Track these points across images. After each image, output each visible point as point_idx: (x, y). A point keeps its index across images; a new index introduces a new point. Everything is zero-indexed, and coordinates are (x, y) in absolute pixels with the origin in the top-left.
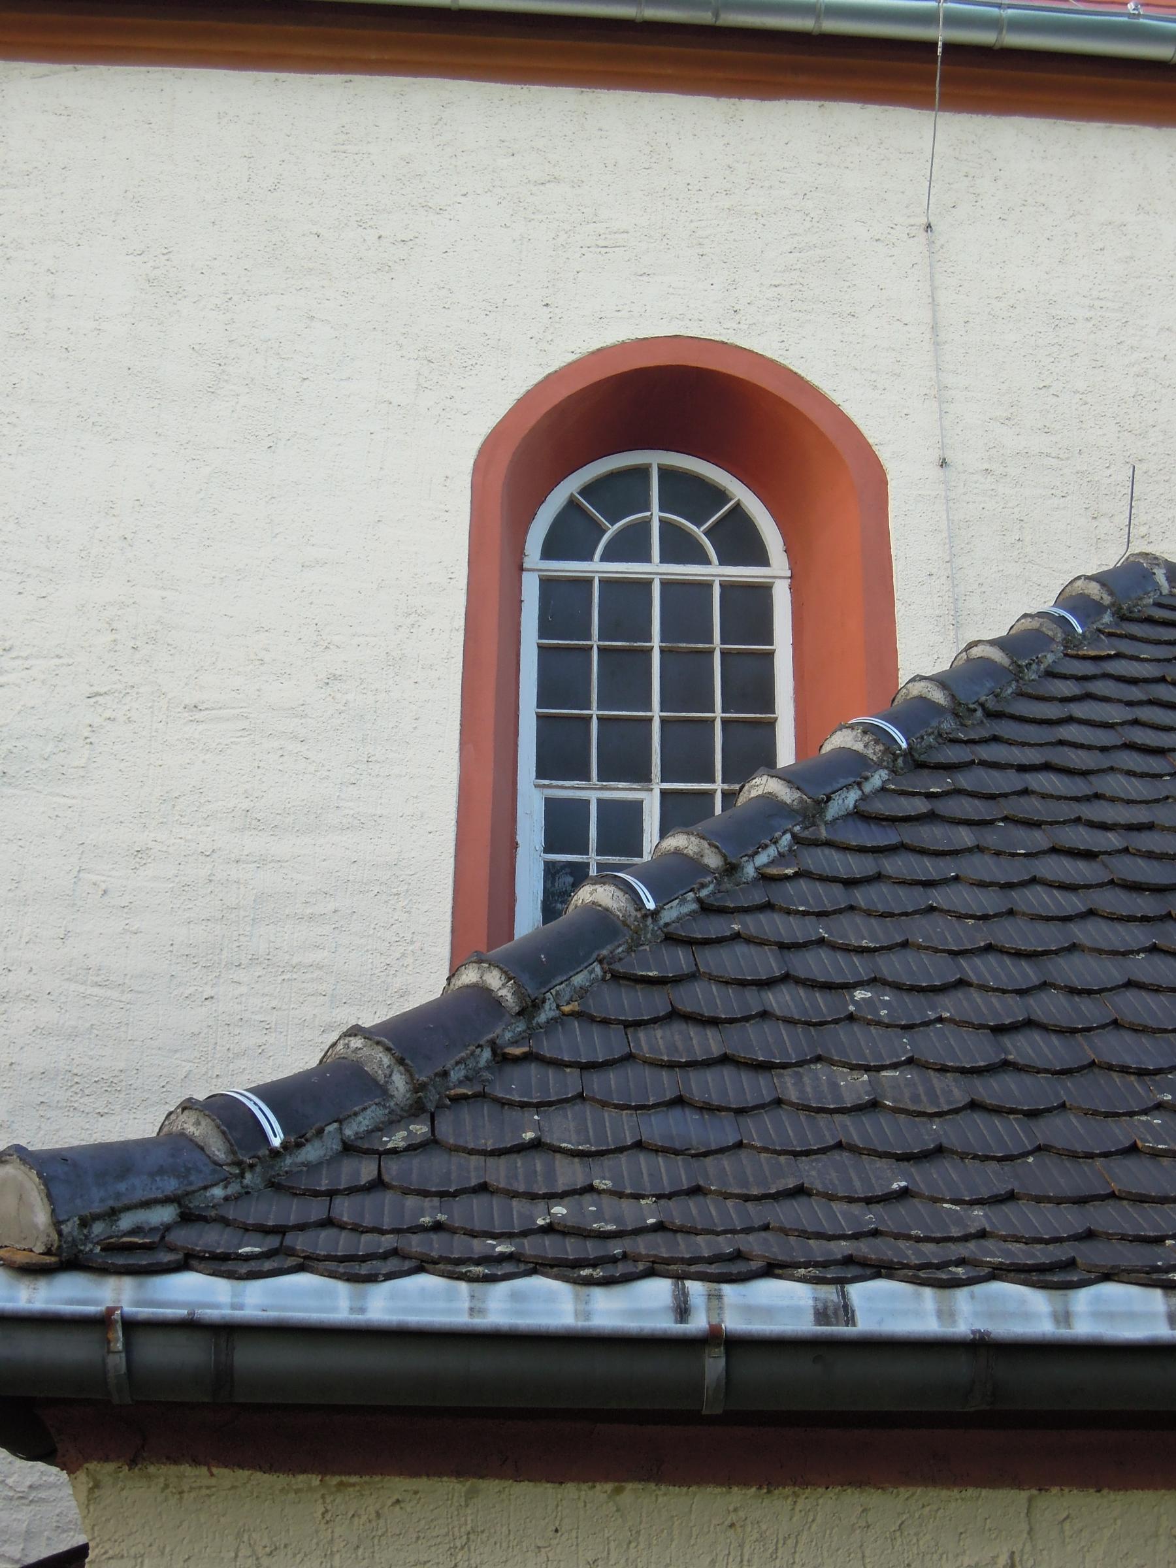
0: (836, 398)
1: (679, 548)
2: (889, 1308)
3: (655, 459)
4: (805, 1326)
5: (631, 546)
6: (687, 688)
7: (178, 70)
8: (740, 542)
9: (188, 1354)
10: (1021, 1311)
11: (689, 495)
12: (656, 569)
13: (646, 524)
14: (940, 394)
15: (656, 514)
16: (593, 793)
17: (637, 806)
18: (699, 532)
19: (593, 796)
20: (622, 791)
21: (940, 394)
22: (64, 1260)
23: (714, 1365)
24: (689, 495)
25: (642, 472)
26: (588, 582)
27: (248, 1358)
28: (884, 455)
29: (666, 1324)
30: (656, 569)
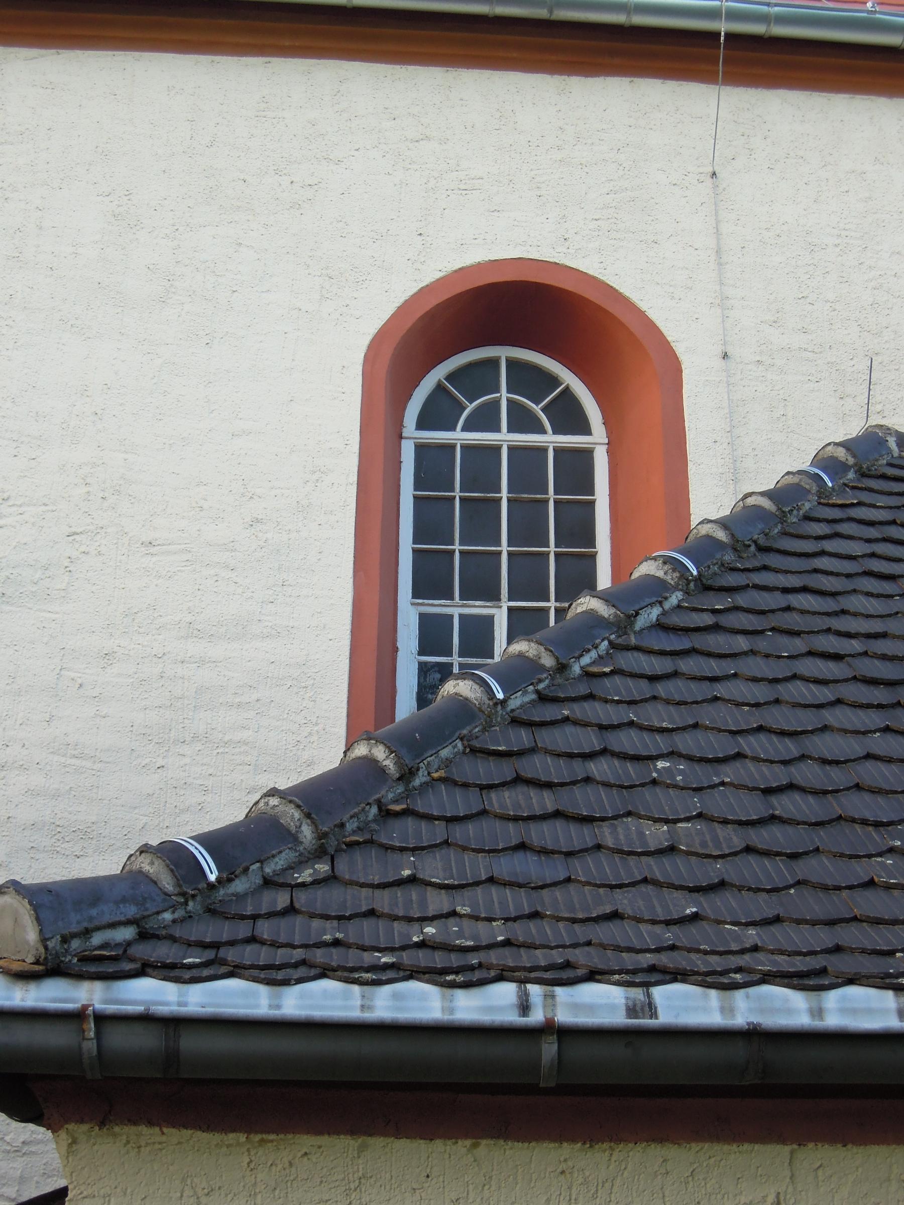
0: (643, 306)
1: (522, 421)
2: (683, 1005)
3: (504, 353)
4: (619, 1019)
5: (485, 419)
6: (528, 528)
7: (137, 54)
8: (569, 417)
9: (145, 1041)
10: (785, 1008)
11: (530, 380)
12: (504, 437)
13: (496, 403)
14: (723, 303)
15: (504, 395)
16: (456, 609)
17: (490, 619)
18: (537, 409)
19: (456, 612)
20: (478, 608)
21: (723, 303)
22: (49, 968)
23: (549, 1049)
24: (530, 380)
25: (494, 363)
26: (452, 447)
27: (190, 1043)
28: (680, 350)
30: (504, 437)
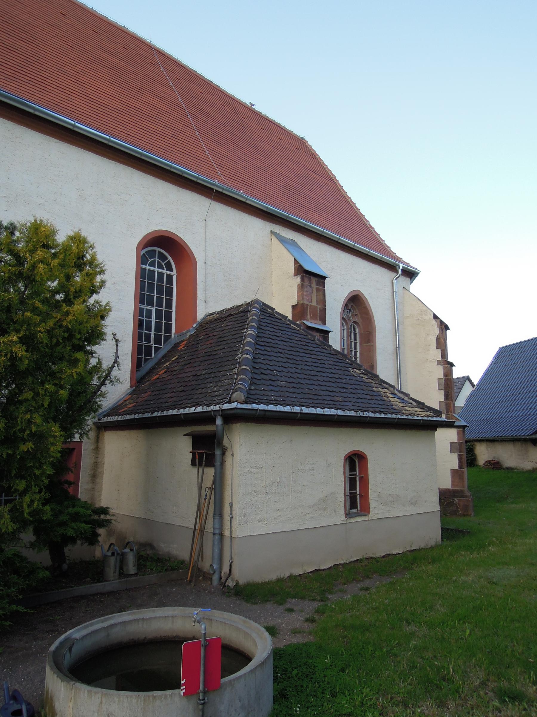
0: (191, 248)
1: (160, 266)
2: (305, 410)
3: (158, 249)
4: (299, 411)
5: (152, 264)
6: (160, 292)
7: (58, 141)
8: (169, 268)
9: (263, 413)
10: (319, 411)
11: (162, 257)
12: (156, 269)
13: (155, 260)
14: (205, 250)
15: (157, 259)
16: (145, 307)
17: (152, 310)
18: (163, 264)
19: (145, 308)
20: (149, 308)
21: (205, 250)
22: (246, 402)
23: (299, 415)
24: (162, 257)
25: (155, 251)
26: (146, 269)
27: (267, 413)
28: (197, 259)
29: (290, 411)
30: (156, 269)
